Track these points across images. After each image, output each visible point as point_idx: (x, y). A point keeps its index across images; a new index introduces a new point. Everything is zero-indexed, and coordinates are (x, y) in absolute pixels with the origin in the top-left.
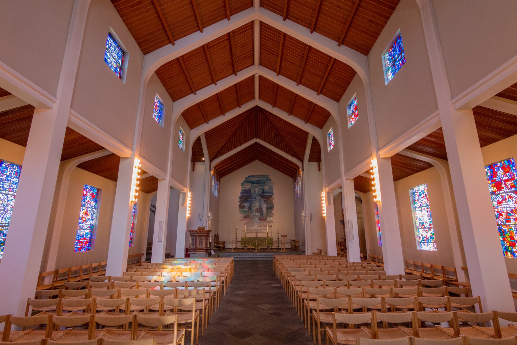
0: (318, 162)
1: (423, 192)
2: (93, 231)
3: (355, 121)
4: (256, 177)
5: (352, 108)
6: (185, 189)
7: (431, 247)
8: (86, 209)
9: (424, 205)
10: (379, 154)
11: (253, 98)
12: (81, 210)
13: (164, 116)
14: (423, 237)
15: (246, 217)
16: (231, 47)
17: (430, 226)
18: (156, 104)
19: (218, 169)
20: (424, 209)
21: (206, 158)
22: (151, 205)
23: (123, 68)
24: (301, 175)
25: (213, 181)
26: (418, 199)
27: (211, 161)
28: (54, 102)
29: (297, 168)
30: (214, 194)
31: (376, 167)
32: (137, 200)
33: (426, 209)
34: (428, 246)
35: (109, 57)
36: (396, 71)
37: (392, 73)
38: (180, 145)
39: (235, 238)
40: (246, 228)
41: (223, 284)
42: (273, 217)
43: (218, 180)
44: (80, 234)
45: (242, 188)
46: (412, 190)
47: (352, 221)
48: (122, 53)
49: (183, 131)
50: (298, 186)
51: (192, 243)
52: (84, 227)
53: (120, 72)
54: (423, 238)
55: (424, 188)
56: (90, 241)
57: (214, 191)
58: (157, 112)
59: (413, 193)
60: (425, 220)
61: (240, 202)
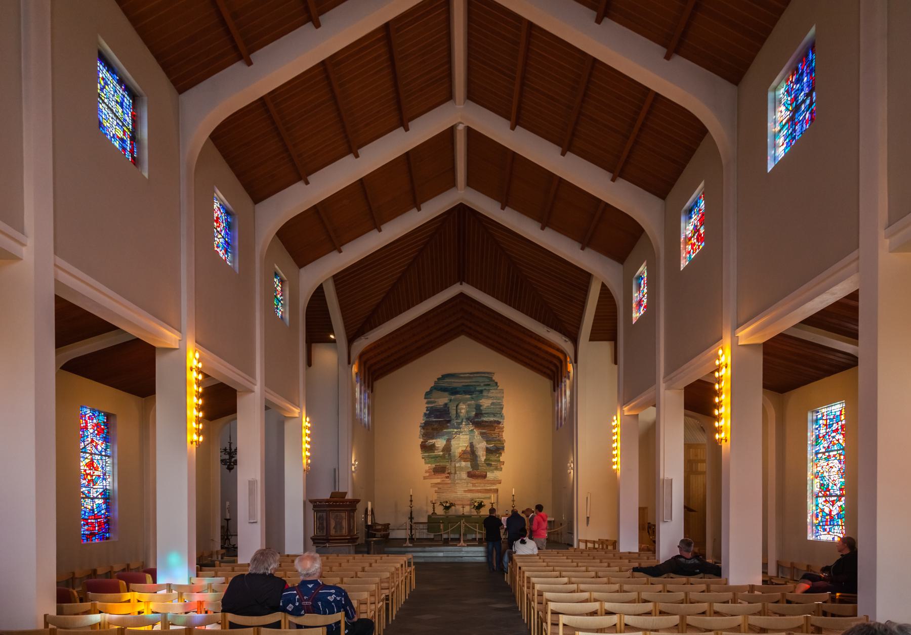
2: (110, 501)
3: (697, 251)
4: (462, 377)
5: (694, 217)
6: (296, 412)
7: (837, 534)
8: (89, 457)
9: (836, 448)
10: (738, 337)
12: (82, 459)
13: (236, 244)
14: (824, 514)
16: (392, 59)
17: (841, 492)
18: (216, 215)
19: (365, 363)
20: (834, 456)
21: (338, 333)
23: (138, 136)
25: (358, 389)
27: (351, 340)
28: (23, 245)
29: (561, 356)
30: (361, 419)
31: (726, 367)
35: (106, 113)
36: (795, 136)
37: (787, 140)
38: (277, 308)
39: (410, 516)
41: (388, 602)
42: (501, 469)
43: (368, 387)
44: (86, 508)
45: (427, 403)
46: (815, 414)
47: (672, 480)
48: (130, 99)
51: (318, 524)
52: (92, 494)
53: (133, 148)
55: (841, 411)
56: (108, 522)
57: (361, 410)
58: (221, 234)
61: (423, 437)
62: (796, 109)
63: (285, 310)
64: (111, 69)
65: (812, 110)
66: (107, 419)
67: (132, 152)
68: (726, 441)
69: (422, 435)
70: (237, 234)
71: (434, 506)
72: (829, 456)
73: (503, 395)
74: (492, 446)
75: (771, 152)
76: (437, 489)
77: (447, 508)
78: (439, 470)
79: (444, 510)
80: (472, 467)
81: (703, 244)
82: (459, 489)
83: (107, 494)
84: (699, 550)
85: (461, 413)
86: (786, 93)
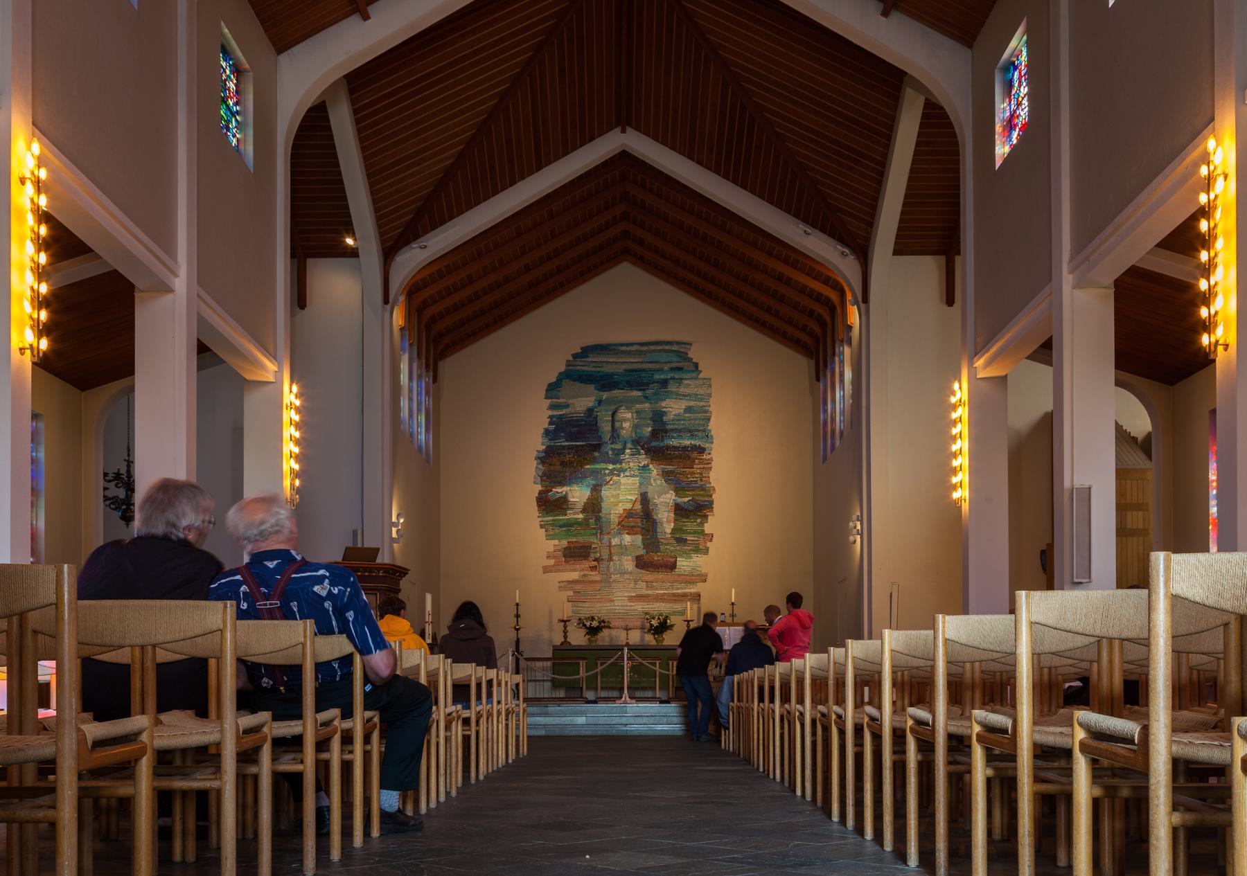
4: (623, 352)
19: (425, 305)
22: (105, 475)
25: (404, 367)
27: (389, 253)
29: (833, 296)
30: (411, 435)
31: (1226, 177)
32: (44, 344)
39: (519, 619)
42: (706, 551)
43: (427, 366)
45: (552, 407)
49: (239, 54)
57: (411, 416)
63: (245, 136)
71: (565, 627)
73: (709, 392)
74: (687, 499)
76: (571, 593)
77: (593, 631)
78: (576, 553)
79: (587, 637)
80: (646, 545)
82: (619, 594)
85: (623, 428)
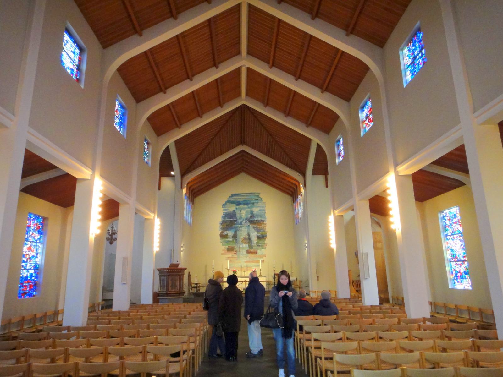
0: (324, 176)
1: (455, 216)
4: (243, 196)
6: (151, 216)
9: (457, 232)
10: (398, 171)
11: (239, 94)
13: (126, 123)
15: (230, 249)
20: (457, 237)
23: (81, 68)
24: (303, 193)
25: (185, 203)
26: (449, 224)
27: (183, 175)
29: (297, 184)
33: (459, 237)
34: (462, 283)
36: (416, 70)
38: (145, 158)
40: (229, 264)
42: (265, 248)
43: (191, 202)
47: (367, 253)
50: (299, 208)
51: (161, 284)
54: (456, 274)
56: (35, 285)
58: (118, 118)
59: (444, 218)
60: (458, 250)
61: (221, 230)
62: (415, 58)
64: (71, 36)
65: (423, 58)
66: (43, 221)
67: (76, 76)
68: (398, 229)
69: (221, 229)
70: (126, 119)
72: (454, 237)
75: (404, 79)
81: (373, 123)
83: (37, 267)
84: (384, 296)
85: (242, 215)
86: (408, 51)
